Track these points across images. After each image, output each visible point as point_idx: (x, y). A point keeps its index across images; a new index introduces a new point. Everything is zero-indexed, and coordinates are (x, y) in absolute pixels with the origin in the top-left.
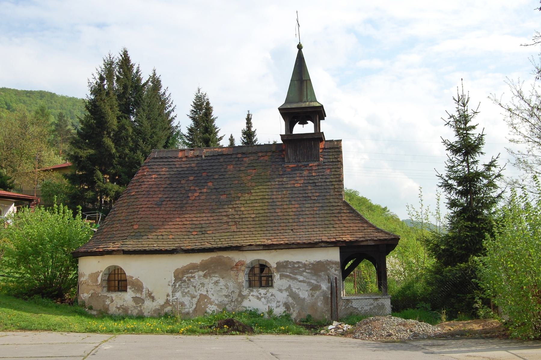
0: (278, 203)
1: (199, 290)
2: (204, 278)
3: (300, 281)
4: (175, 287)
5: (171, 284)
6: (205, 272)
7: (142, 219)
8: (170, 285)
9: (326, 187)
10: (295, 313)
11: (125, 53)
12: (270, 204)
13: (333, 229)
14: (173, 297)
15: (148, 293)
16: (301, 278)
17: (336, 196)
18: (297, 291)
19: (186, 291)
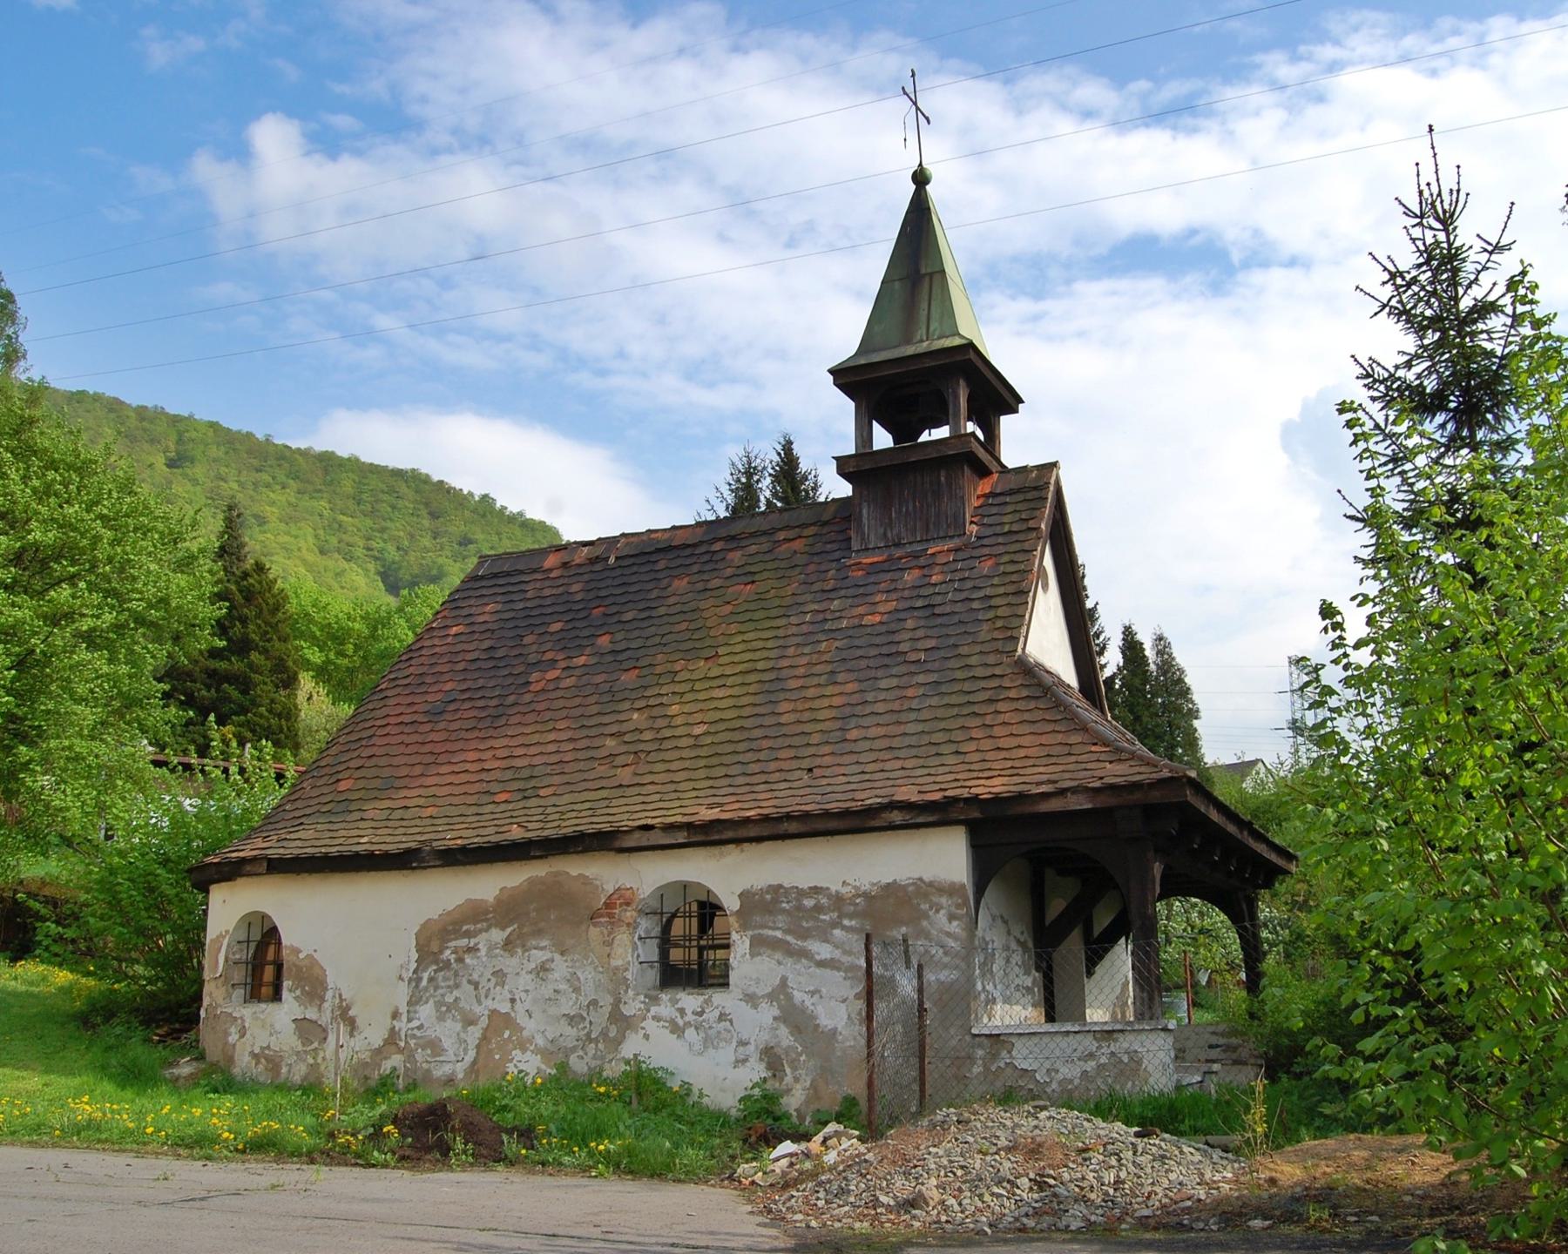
0: (793, 684)
1: (486, 997)
2: (506, 954)
3: (822, 964)
4: (417, 986)
5: (407, 975)
6: (509, 930)
7: (374, 759)
8: (403, 980)
9: (964, 617)
10: (798, 1086)
11: (788, 446)
12: (767, 687)
13: (952, 760)
14: (409, 1020)
15: (340, 1007)
16: (824, 951)
17: (995, 643)
18: (808, 1003)
19: (449, 999)
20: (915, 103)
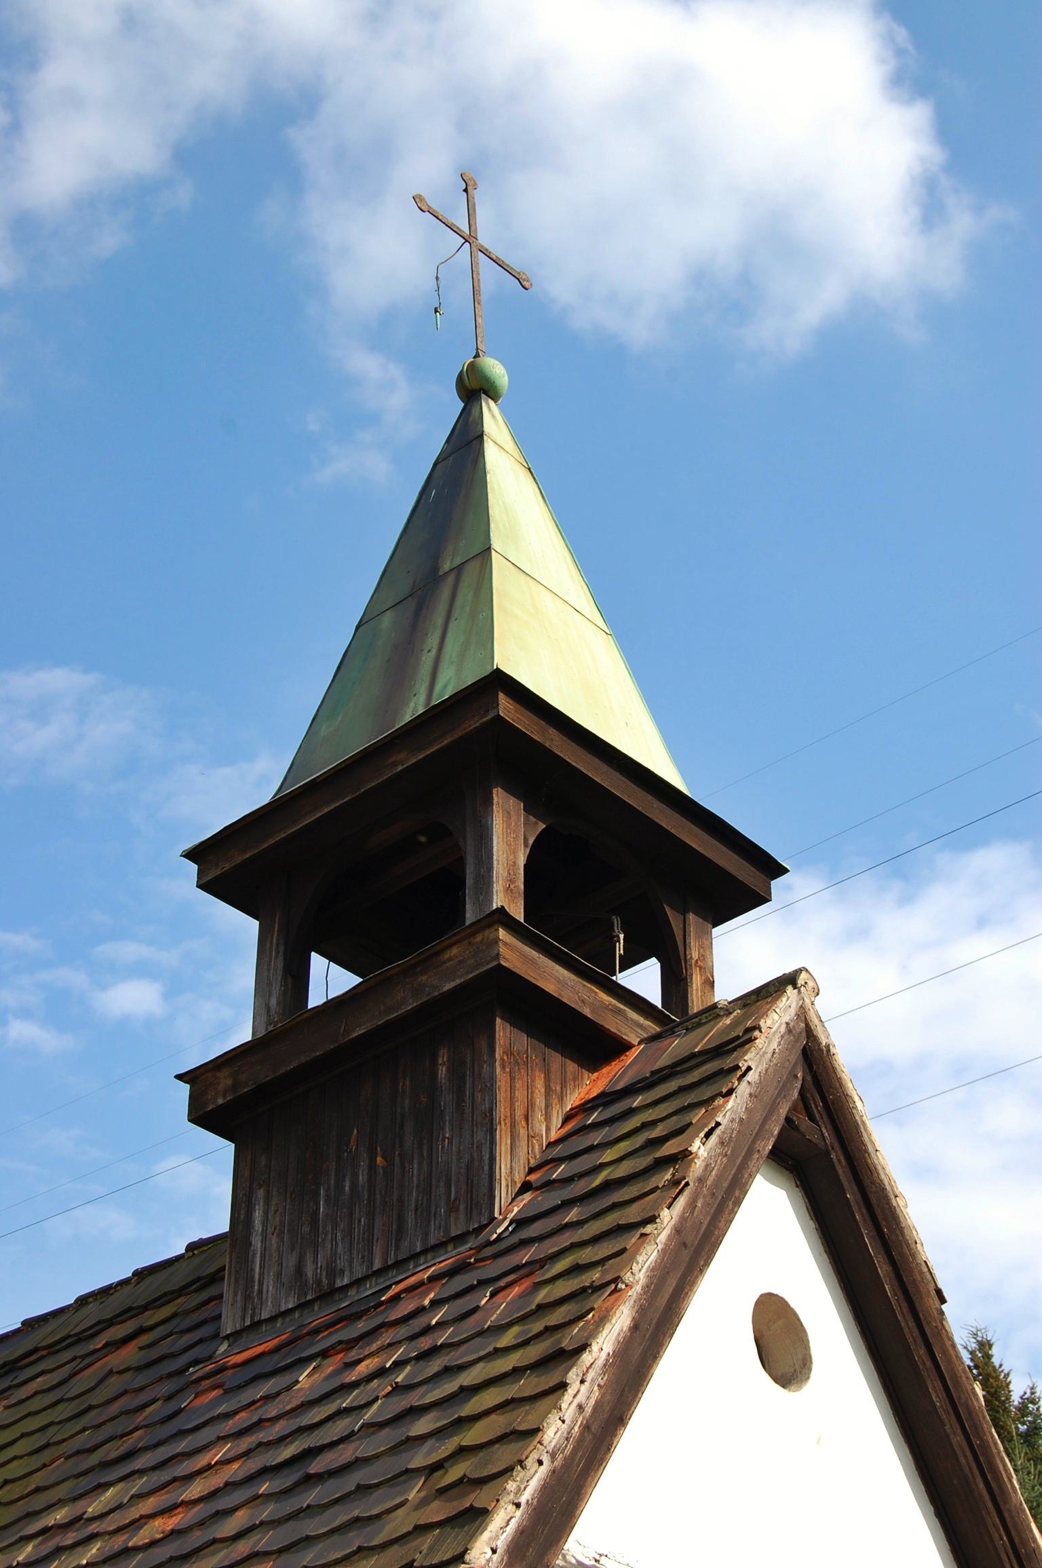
20: (469, 239)
